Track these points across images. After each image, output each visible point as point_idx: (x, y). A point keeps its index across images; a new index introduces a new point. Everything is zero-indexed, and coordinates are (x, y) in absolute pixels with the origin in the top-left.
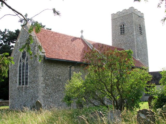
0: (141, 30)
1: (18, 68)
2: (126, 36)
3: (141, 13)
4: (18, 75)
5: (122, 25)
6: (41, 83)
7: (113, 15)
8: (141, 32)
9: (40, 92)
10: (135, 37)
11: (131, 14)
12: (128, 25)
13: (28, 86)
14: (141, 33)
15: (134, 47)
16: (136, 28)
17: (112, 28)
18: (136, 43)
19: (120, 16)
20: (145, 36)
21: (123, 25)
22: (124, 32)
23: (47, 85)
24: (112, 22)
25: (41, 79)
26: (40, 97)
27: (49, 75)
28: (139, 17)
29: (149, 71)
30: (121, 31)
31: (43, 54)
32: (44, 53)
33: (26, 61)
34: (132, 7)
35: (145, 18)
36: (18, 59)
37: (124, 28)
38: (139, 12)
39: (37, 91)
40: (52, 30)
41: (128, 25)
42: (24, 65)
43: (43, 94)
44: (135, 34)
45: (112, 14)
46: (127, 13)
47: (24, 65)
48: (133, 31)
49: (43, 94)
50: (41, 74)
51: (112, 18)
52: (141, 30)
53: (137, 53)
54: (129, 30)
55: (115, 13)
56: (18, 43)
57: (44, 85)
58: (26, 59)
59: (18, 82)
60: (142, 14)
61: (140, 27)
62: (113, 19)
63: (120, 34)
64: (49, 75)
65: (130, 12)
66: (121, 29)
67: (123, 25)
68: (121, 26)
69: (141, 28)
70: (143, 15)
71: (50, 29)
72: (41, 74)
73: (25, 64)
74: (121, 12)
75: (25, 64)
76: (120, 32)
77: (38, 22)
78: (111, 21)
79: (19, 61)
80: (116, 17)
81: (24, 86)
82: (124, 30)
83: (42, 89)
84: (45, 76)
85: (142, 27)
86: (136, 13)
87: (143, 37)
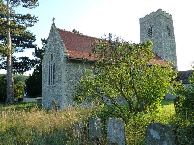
0: (169, 31)
1: (48, 69)
2: (153, 38)
3: (170, 15)
4: (48, 75)
5: (150, 28)
6: (64, 82)
7: (141, 19)
8: (170, 33)
9: (63, 90)
10: (163, 38)
11: (159, 16)
12: (158, 26)
13: (54, 85)
14: (169, 34)
15: (162, 48)
16: (164, 29)
17: (140, 31)
18: (164, 44)
19: (148, 19)
20: (174, 37)
21: (151, 28)
22: (152, 34)
23: (70, 84)
24: (140, 25)
25: (64, 78)
26: (63, 96)
27: (72, 74)
28: (167, 18)
29: (177, 70)
30: (149, 33)
31: (66, 54)
32: (67, 53)
33: (53, 62)
34: (160, 9)
35: (173, 19)
36: (48, 61)
37: (152, 30)
38: (167, 13)
39: (61, 90)
40: (83, 34)
41: (158, 26)
42: (52, 65)
43: (66, 93)
44: (162, 35)
45: (140, 18)
46: (155, 15)
47: (52, 65)
48: (161, 33)
49: (66, 93)
50: (64, 73)
51: (140, 22)
52: (170, 31)
53: (165, 53)
54: (156, 32)
55: (143, 17)
56: (48, 46)
57: (67, 84)
58: (53, 60)
59: (48, 82)
60: (171, 15)
61: (168, 29)
62: (142, 23)
63: (148, 36)
64: (72, 74)
65: (158, 14)
66: (149, 31)
67: (151, 28)
68: (149, 28)
69: (169, 29)
70: (172, 17)
71: (82, 34)
72: (64, 73)
73: (53, 65)
74: (149, 15)
75: (53, 65)
76: (148, 34)
77: (75, 30)
78: (139, 25)
79: (49, 62)
80: (144, 21)
81: (52, 85)
82: (151, 33)
83: (65, 88)
84: (68, 75)
85: (170, 28)
86: (164, 15)
87: (171, 38)
